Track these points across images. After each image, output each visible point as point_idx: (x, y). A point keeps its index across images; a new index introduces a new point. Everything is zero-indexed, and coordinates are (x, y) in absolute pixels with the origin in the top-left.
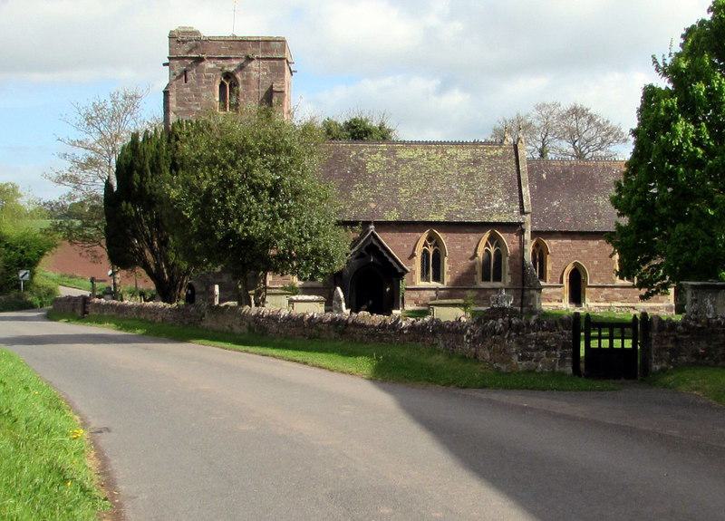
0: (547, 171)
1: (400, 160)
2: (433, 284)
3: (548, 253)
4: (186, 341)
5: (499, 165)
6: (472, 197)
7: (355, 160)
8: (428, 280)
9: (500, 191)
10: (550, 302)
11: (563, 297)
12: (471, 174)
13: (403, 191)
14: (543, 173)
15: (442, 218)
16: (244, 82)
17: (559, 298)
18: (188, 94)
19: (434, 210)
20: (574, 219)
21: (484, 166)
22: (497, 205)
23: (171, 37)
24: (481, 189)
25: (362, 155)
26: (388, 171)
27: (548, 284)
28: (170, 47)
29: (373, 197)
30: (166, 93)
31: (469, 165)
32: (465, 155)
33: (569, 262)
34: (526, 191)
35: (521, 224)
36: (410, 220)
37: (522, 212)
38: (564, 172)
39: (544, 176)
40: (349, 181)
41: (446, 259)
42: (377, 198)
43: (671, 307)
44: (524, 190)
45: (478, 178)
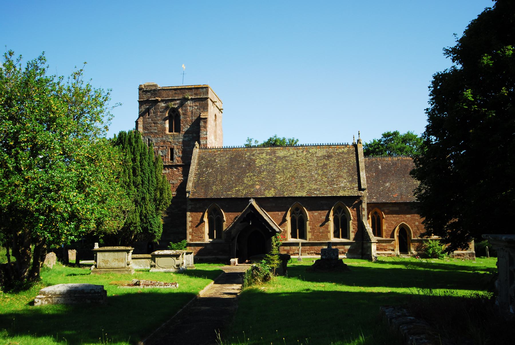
0: (382, 164)
1: (279, 158)
2: (298, 240)
3: (383, 218)
4: (95, 285)
5: (345, 158)
6: (325, 179)
7: (248, 158)
8: (338, 237)
9: (345, 175)
10: (385, 251)
11: (395, 247)
12: (325, 165)
13: (279, 177)
14: (379, 165)
15: (304, 194)
16: (184, 114)
17: (392, 248)
18: (150, 123)
19: (299, 189)
20: (401, 194)
21: (334, 159)
22: (343, 185)
23: (140, 89)
24: (332, 174)
25: (253, 155)
26: (270, 164)
27: (384, 239)
28: (139, 95)
29: (258, 181)
30: (137, 122)
31: (324, 158)
32: (321, 153)
33: (398, 223)
34: (363, 174)
35: (358, 197)
36: (282, 196)
37: (360, 189)
38: (393, 164)
39: (380, 167)
40: (244, 172)
41: (308, 222)
42: (262, 183)
43: (472, 254)
44: (361, 174)
45: (330, 167)
